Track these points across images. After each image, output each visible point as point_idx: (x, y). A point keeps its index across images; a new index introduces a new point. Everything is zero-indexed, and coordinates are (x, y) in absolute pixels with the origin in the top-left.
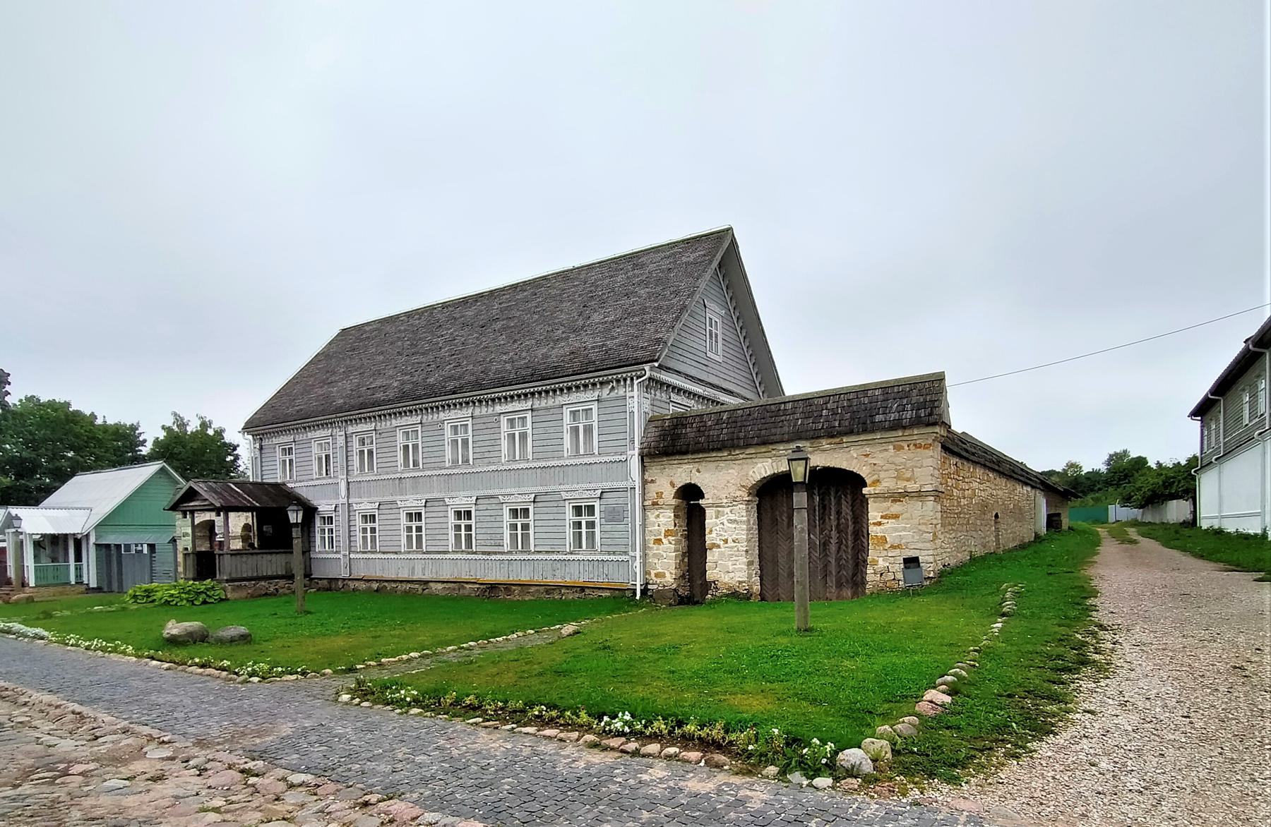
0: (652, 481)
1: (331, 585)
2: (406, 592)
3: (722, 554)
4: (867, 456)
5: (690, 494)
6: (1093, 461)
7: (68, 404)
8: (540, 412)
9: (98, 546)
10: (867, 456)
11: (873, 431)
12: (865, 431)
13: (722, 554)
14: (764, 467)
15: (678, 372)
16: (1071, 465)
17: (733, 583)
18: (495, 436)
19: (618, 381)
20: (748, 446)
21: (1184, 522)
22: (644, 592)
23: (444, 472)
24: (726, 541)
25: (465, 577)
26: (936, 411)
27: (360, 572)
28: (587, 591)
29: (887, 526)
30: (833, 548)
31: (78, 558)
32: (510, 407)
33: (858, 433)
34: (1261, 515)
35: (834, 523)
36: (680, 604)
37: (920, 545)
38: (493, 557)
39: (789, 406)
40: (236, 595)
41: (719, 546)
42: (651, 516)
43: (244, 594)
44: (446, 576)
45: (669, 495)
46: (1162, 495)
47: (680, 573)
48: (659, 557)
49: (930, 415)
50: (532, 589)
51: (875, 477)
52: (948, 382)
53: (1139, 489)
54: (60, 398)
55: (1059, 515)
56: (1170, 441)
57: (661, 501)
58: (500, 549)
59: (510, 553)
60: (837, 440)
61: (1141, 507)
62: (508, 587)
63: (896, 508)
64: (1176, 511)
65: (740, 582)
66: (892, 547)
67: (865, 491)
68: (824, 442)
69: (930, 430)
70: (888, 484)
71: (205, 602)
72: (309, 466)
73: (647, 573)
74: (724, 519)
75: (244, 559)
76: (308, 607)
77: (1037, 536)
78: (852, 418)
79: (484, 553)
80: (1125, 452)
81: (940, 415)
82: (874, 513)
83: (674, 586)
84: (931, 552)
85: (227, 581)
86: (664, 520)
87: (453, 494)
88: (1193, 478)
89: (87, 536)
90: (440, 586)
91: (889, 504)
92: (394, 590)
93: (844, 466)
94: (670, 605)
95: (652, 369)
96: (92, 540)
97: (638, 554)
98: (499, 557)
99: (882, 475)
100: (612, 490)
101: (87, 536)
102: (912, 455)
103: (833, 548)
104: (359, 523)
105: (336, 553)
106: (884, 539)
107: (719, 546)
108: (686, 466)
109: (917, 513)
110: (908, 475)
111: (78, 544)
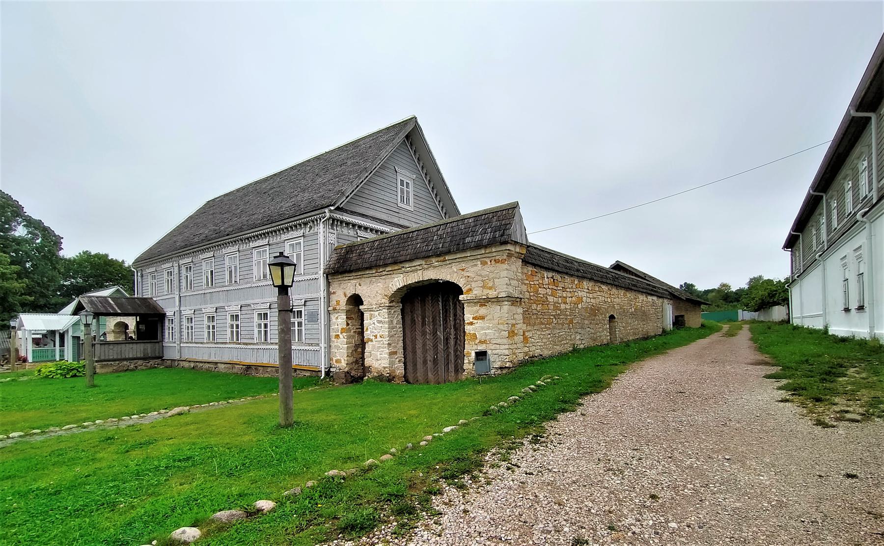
0: (334, 293)
1: (172, 365)
2: (207, 370)
3: (374, 346)
4: (463, 270)
5: (356, 300)
6: (738, 283)
7: (107, 256)
8: (274, 246)
9: (73, 337)
10: (463, 270)
11: (464, 250)
12: (458, 251)
13: (374, 346)
14: (398, 281)
15: (363, 215)
16: (724, 285)
17: (380, 368)
18: (250, 264)
19: (313, 222)
20: (386, 265)
21: (782, 321)
22: (328, 373)
23: (225, 289)
24: (376, 337)
25: (235, 360)
26: (507, 232)
27: (186, 355)
28: (298, 372)
29: (477, 325)
30: (452, 342)
31: (62, 344)
32: (257, 244)
33: (455, 253)
34: (824, 315)
35: (452, 323)
36: (352, 382)
37: (499, 341)
38: (249, 347)
39: (415, 233)
40: (104, 371)
41: (372, 341)
42: (333, 317)
43: (111, 369)
44: (226, 360)
45: (343, 301)
46: (768, 303)
47: (352, 359)
48: (338, 348)
49: (502, 236)
50: (269, 369)
51: (469, 287)
52: (523, 210)
53: (753, 299)
54: (102, 252)
55: (682, 316)
56: (778, 267)
57: (338, 307)
58: (201, 341)
59: (257, 343)
60: (442, 258)
61: (756, 311)
62: (257, 367)
63: (483, 311)
64: (777, 313)
65: (385, 368)
66: (481, 342)
67: (461, 297)
68: (434, 260)
69: (503, 248)
70: (477, 292)
71: (75, 376)
72: (153, 288)
73: (331, 359)
74: (375, 320)
75: (111, 347)
76: (96, 382)
77: (664, 332)
78: (451, 241)
79: (244, 344)
80: (760, 277)
81: (509, 235)
82: (468, 317)
83: (346, 370)
84: (507, 347)
85: (97, 361)
86: (340, 321)
87: (229, 304)
88: (787, 290)
89: (67, 331)
90: (223, 366)
91: (478, 308)
92: (201, 368)
93: (448, 278)
94: (343, 383)
95: (331, 211)
96: (70, 333)
97: (323, 345)
98: (252, 347)
99: (473, 285)
100: (312, 300)
101: (67, 331)
102: (493, 269)
103: (452, 342)
104: (185, 323)
105: (177, 343)
106: (475, 335)
107: (372, 341)
108: (353, 281)
109: (497, 315)
110: (490, 284)
111: (62, 336)
